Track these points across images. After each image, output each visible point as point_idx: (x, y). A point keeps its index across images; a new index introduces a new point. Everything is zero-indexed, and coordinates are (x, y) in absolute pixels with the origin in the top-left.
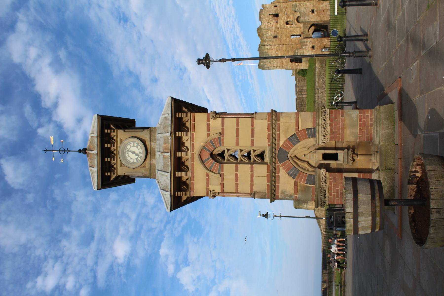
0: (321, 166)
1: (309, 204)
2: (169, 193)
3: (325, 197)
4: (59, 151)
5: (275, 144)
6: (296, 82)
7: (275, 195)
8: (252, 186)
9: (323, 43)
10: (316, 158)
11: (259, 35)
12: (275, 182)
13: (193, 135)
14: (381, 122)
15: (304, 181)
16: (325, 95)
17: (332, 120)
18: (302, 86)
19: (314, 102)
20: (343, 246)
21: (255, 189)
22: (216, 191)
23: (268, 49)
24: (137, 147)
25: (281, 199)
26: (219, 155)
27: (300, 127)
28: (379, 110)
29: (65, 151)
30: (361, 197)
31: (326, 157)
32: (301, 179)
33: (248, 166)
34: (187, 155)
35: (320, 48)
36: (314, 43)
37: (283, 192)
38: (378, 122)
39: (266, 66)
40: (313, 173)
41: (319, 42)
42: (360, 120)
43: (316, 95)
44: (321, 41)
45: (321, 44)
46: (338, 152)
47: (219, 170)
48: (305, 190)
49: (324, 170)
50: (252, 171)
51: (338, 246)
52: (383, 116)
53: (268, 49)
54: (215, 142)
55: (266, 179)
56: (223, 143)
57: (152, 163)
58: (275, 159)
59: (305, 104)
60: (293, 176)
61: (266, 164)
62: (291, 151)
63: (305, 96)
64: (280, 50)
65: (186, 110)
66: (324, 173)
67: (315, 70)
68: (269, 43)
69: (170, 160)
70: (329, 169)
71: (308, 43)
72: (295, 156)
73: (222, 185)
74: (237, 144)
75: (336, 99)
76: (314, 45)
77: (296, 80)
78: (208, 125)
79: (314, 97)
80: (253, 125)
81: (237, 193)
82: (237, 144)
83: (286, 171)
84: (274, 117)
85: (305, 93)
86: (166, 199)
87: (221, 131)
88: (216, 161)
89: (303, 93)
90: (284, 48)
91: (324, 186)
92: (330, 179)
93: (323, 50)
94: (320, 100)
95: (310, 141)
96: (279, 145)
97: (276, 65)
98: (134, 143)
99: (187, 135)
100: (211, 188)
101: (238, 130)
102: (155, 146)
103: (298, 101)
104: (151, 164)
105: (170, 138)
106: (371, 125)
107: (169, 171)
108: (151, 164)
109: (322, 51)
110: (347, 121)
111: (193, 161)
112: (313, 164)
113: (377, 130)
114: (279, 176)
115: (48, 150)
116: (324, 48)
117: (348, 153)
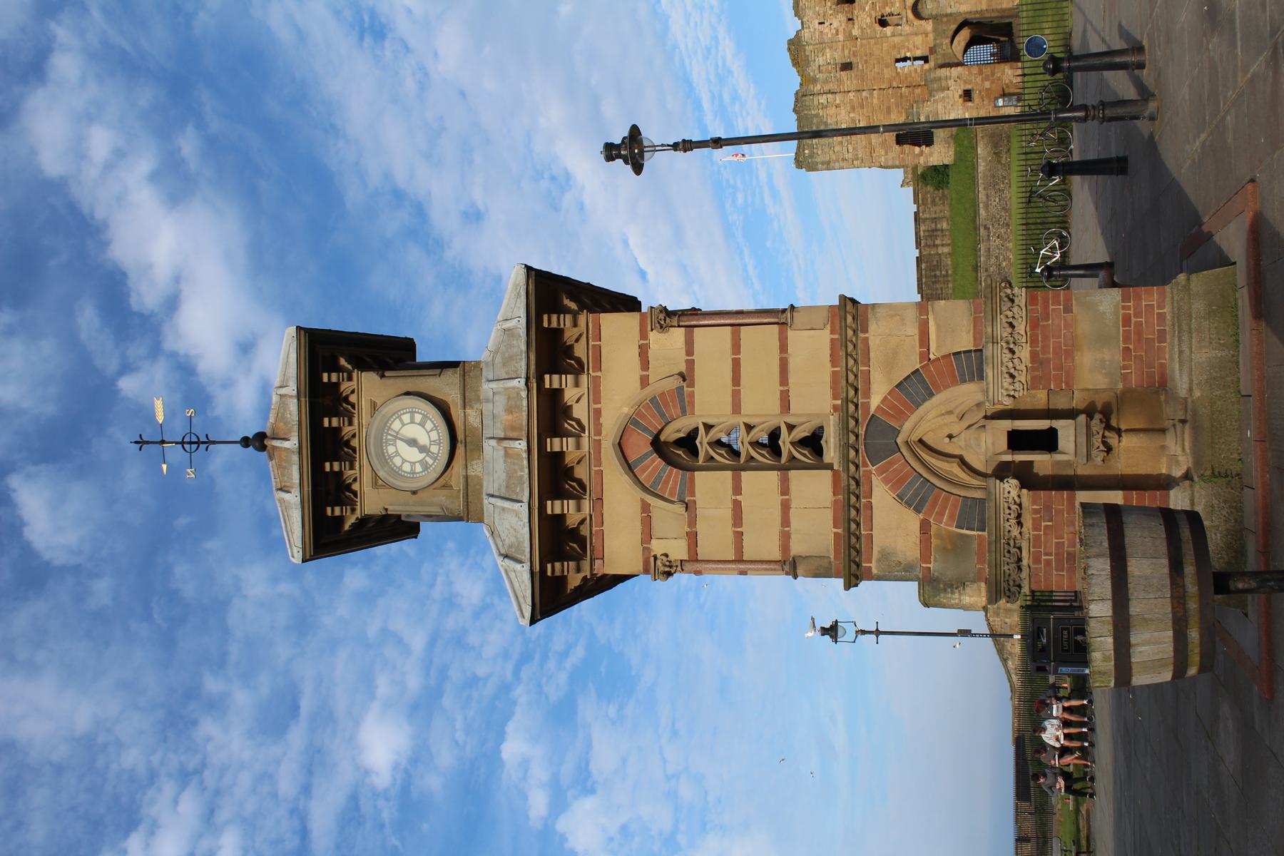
0: (1002, 471)
1: (968, 590)
2: (527, 566)
3: (1019, 568)
4: (182, 443)
5: (856, 406)
6: (915, 208)
7: (858, 565)
8: (785, 538)
9: (999, 79)
10: (989, 445)
11: (796, 63)
12: (858, 525)
13: (596, 382)
14: (1194, 326)
15: (951, 517)
16: (1011, 245)
17: (1034, 324)
18: (934, 220)
19: (976, 268)
20: (1082, 724)
21: (796, 549)
22: (672, 558)
23: (825, 107)
24: (422, 424)
25: (879, 578)
26: (679, 443)
27: (932, 349)
28: (1187, 288)
29: (198, 443)
30: (1137, 567)
31: (1017, 441)
32: (941, 514)
33: (774, 476)
34: (578, 447)
35: (988, 96)
36: (970, 82)
37: (885, 556)
38: (1185, 327)
39: (818, 160)
40: (978, 494)
41: (987, 78)
42: (1127, 321)
43: (982, 247)
44: (993, 74)
45: (992, 82)
46: (1058, 424)
47: (682, 493)
48: (956, 546)
49: (1014, 482)
50: (785, 490)
51: (1066, 724)
52: (1199, 306)
53: (825, 107)
54: (666, 405)
55: (829, 515)
56: (692, 404)
57: (471, 473)
58: (857, 451)
59: (947, 275)
60: (916, 504)
61: (829, 467)
62: (908, 425)
63: (946, 250)
64: (862, 107)
65: (573, 306)
66: (1014, 493)
67: (974, 167)
68: (826, 88)
69: (525, 463)
70: (1028, 478)
71: (951, 83)
72: (921, 441)
73: (693, 538)
74: (736, 408)
75: (1046, 258)
76: (969, 87)
77: (916, 201)
78: (643, 351)
79: (976, 251)
80: (783, 347)
81: (740, 562)
82: (736, 408)
83: (893, 488)
84: (849, 319)
85: (947, 241)
86: (517, 585)
87: (683, 368)
88: (670, 461)
89: (938, 242)
90: (875, 101)
91: (1015, 532)
92: (1035, 512)
93: (1000, 102)
94: (993, 260)
95: (967, 393)
96: (867, 406)
97: (850, 156)
98: (412, 413)
99: (577, 385)
100: (657, 547)
101: (736, 364)
102: (479, 420)
103: (923, 266)
104: (467, 477)
105: (524, 394)
106: (1162, 336)
107: (526, 498)
108: (467, 477)
109: (996, 107)
110: (1084, 325)
111: (599, 463)
112: (979, 466)
113: (1181, 352)
114: (870, 506)
115: (147, 443)
116: (1004, 95)
117: (1088, 427)
